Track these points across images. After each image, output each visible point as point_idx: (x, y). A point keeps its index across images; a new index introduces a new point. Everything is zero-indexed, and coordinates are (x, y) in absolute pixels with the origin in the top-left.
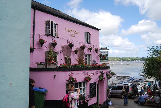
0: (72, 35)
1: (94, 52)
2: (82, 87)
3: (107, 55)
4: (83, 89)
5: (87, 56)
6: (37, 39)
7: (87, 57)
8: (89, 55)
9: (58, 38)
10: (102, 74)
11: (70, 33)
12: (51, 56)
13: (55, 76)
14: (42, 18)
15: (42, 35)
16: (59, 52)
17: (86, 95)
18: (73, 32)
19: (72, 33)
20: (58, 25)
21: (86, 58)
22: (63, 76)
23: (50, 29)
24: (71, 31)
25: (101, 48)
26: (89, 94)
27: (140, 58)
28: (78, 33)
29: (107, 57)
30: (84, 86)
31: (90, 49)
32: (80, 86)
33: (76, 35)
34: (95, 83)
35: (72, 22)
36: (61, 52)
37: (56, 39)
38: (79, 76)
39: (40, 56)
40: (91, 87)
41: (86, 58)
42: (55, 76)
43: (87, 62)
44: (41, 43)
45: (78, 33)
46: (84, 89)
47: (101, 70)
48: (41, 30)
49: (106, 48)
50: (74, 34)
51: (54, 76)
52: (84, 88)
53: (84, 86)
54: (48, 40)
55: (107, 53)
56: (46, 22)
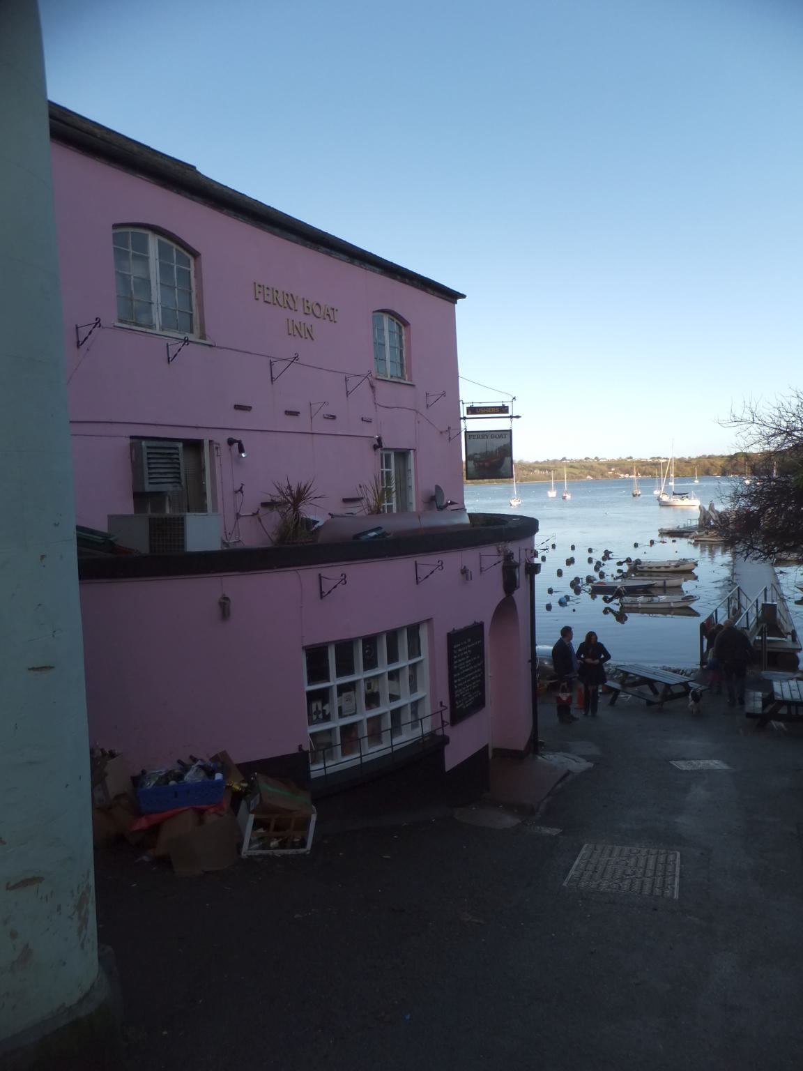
0: (297, 331)
2: (404, 662)
3: (507, 451)
4: (407, 672)
5: (388, 457)
7: (388, 466)
9: (272, 383)
13: (224, 606)
15: (98, 323)
18: (299, 306)
19: (299, 317)
20: (204, 259)
21: (385, 470)
24: (289, 302)
25: (472, 410)
28: (330, 315)
29: (507, 459)
32: (393, 658)
35: (294, 237)
42: (224, 606)
43: (393, 481)
45: (330, 315)
49: (503, 409)
50: (310, 320)
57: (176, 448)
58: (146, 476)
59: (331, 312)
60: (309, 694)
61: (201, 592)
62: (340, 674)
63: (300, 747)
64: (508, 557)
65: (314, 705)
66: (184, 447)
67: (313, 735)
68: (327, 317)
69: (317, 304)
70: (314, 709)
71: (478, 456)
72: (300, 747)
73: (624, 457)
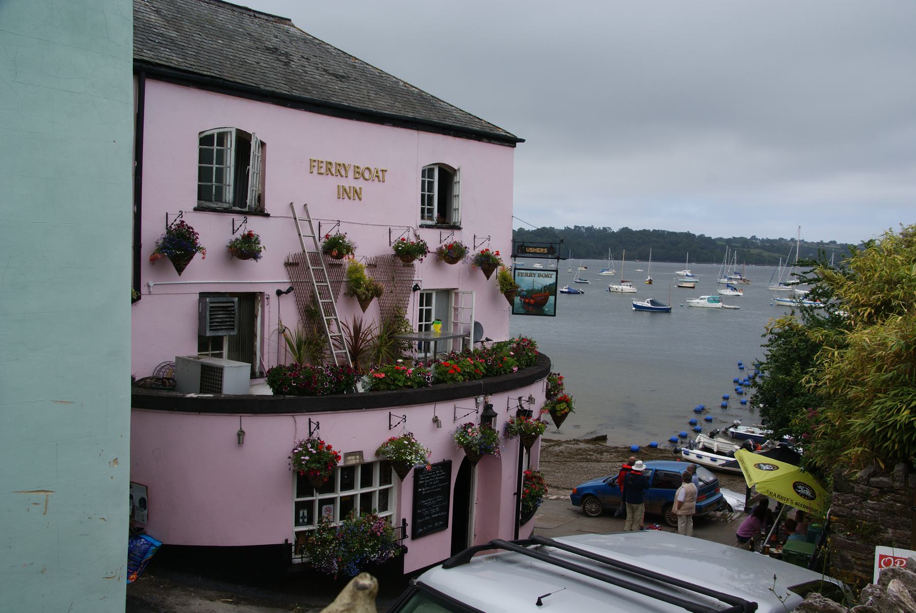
0: (344, 193)
1: (472, 272)
2: (376, 487)
5: (429, 296)
6: (154, 232)
7: (429, 303)
8: (446, 293)
10: (488, 416)
11: (334, 182)
12: (229, 320)
13: (241, 434)
14: (184, 117)
16: (270, 291)
17: (393, 525)
18: (351, 174)
19: (350, 182)
21: (425, 308)
22: (277, 437)
23: (229, 174)
24: (339, 169)
26: (409, 521)
27: (841, 245)
29: (552, 298)
30: (385, 479)
31: (452, 254)
33: (368, 188)
34: (446, 466)
36: (279, 293)
37: (255, 225)
38: (356, 434)
39: (168, 331)
40: (423, 486)
41: (425, 308)
42: (241, 434)
44: (179, 247)
45: (380, 176)
46: (384, 494)
47: (481, 399)
48: (173, 192)
51: (239, 435)
52: (387, 490)
53: (385, 479)
54: (214, 232)
55: (550, 281)
56: (205, 140)
57: (233, 302)
58: (208, 325)
59: (380, 174)
60: (297, 503)
61: (228, 424)
62: (362, 486)
63: (287, 540)
64: (488, 407)
65: (301, 512)
66: (239, 301)
67: (298, 534)
68: (376, 179)
69: (368, 168)
70: (301, 515)
71: (525, 293)
72: (287, 540)
73: (826, 241)
